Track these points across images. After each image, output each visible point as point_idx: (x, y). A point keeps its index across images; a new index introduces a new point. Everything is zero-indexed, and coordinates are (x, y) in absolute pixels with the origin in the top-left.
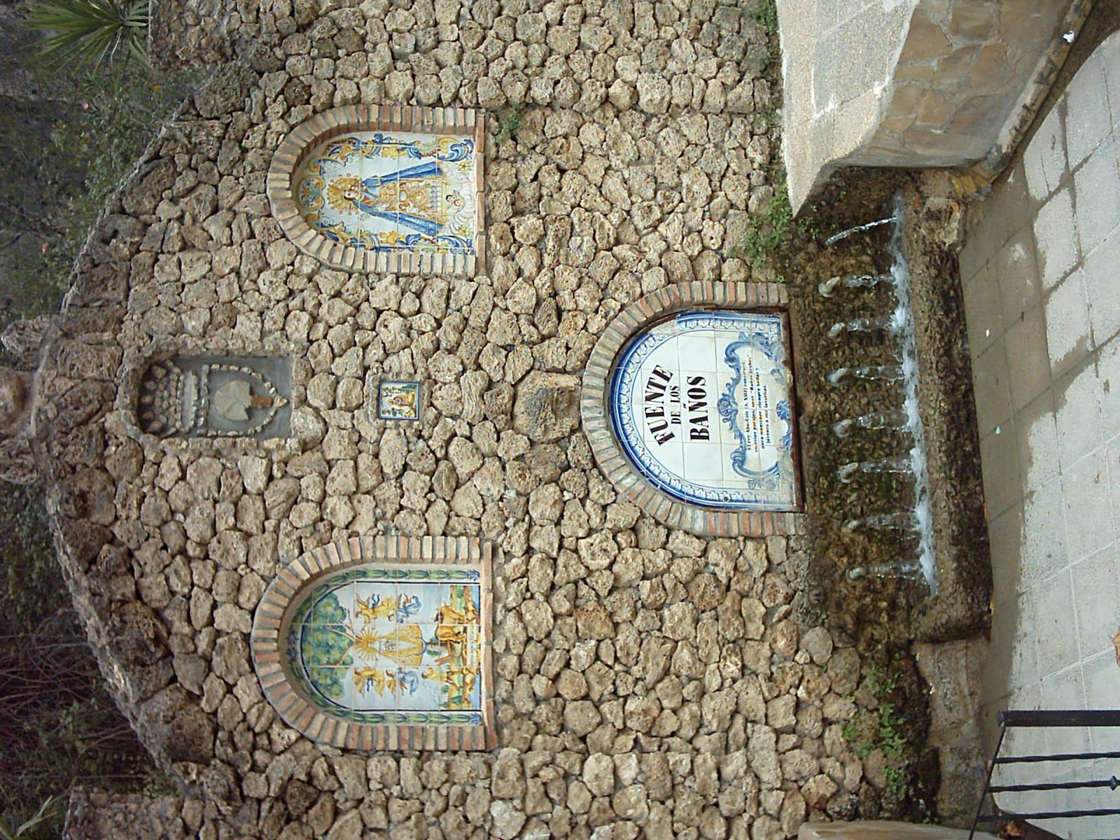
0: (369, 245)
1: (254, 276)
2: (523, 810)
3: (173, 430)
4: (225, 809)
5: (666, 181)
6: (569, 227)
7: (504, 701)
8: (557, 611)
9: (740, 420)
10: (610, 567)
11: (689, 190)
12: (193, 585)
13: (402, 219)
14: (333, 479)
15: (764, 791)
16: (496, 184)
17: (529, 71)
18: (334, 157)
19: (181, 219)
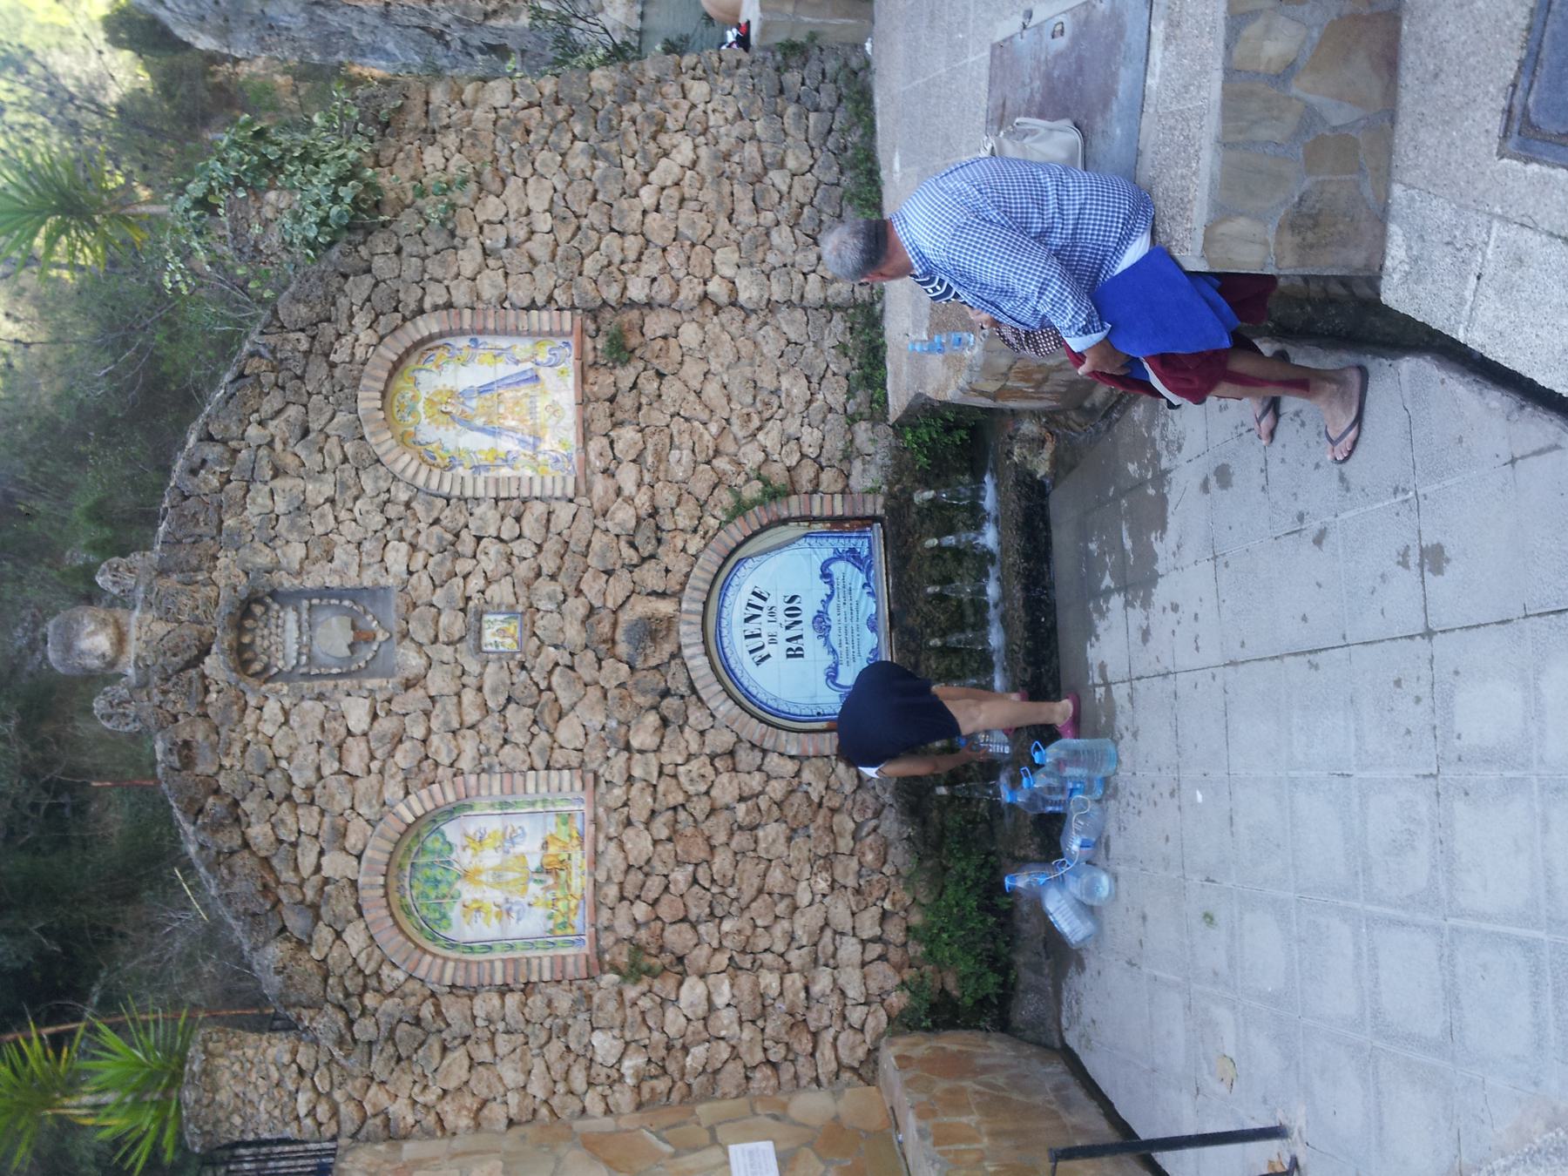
3: (275, 670)
4: (337, 1053)
6: (667, 441)
7: (606, 928)
9: (833, 636)
10: (707, 793)
12: (299, 832)
17: (624, 268)
18: (428, 366)
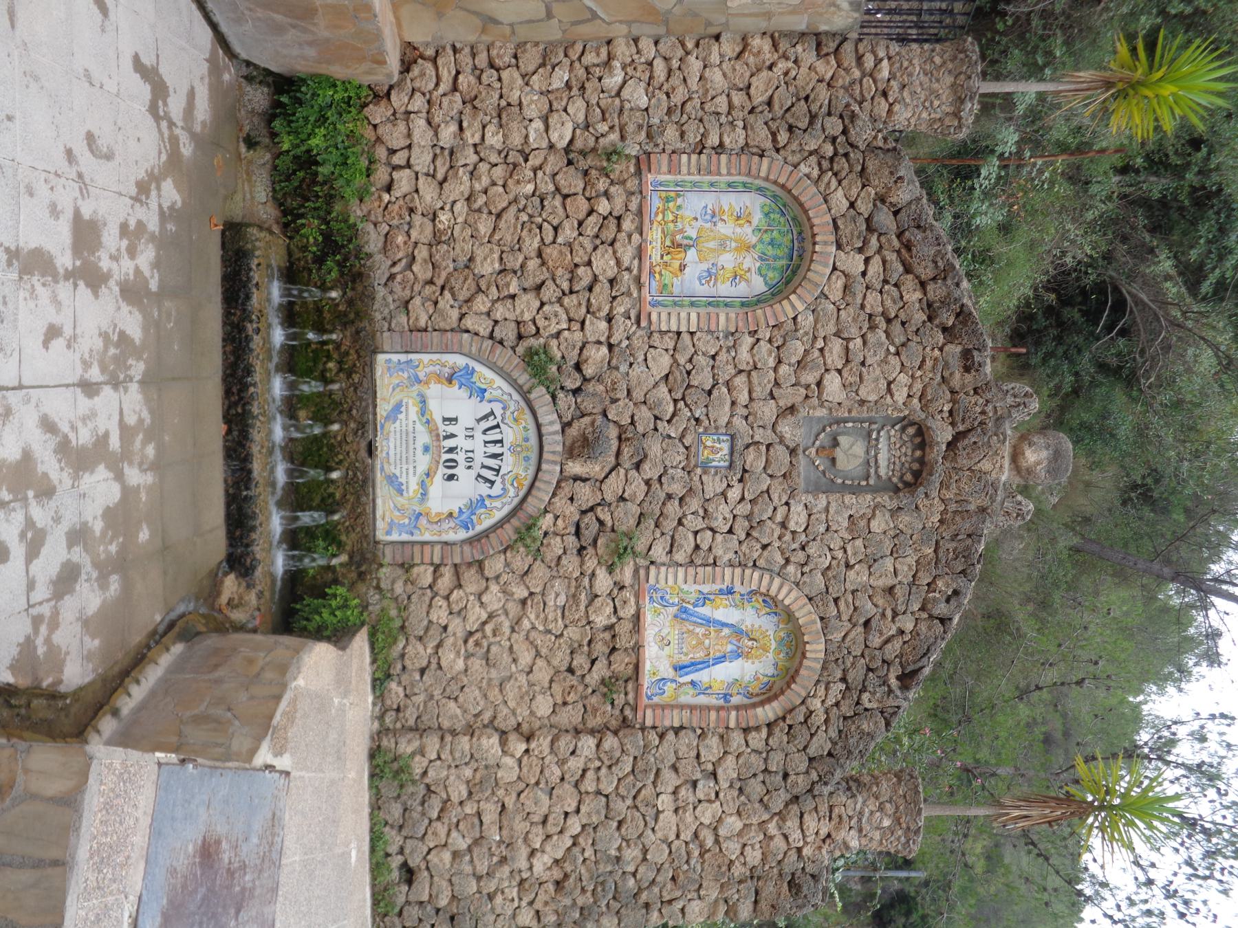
1: (834, 562)
2: (622, 101)
3: (897, 427)
4: (856, 108)
6: (567, 613)
7: (633, 193)
8: (588, 268)
10: (542, 304)
11: (458, 653)
12: (881, 292)
13: (708, 621)
15: (424, 111)
16: (629, 655)
17: (598, 764)
18: (766, 680)
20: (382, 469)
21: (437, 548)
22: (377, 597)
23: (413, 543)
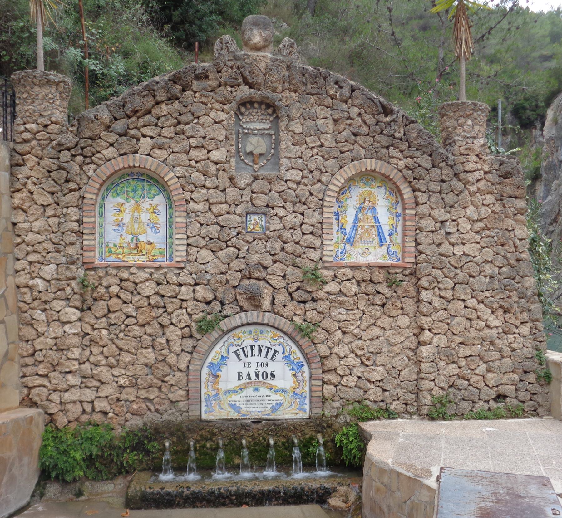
0: (340, 210)
1: (320, 154)
2: (53, 279)
3: (241, 118)
4: (54, 143)
5: (378, 358)
6: (350, 308)
7: (107, 272)
10: (172, 324)
12: (162, 128)
13: (354, 226)
14: (215, 192)
16: (374, 272)
17: (436, 289)
18: (388, 193)
19: (349, 118)
20: (268, 415)
21: (314, 383)
22: (341, 417)
23: (311, 396)
